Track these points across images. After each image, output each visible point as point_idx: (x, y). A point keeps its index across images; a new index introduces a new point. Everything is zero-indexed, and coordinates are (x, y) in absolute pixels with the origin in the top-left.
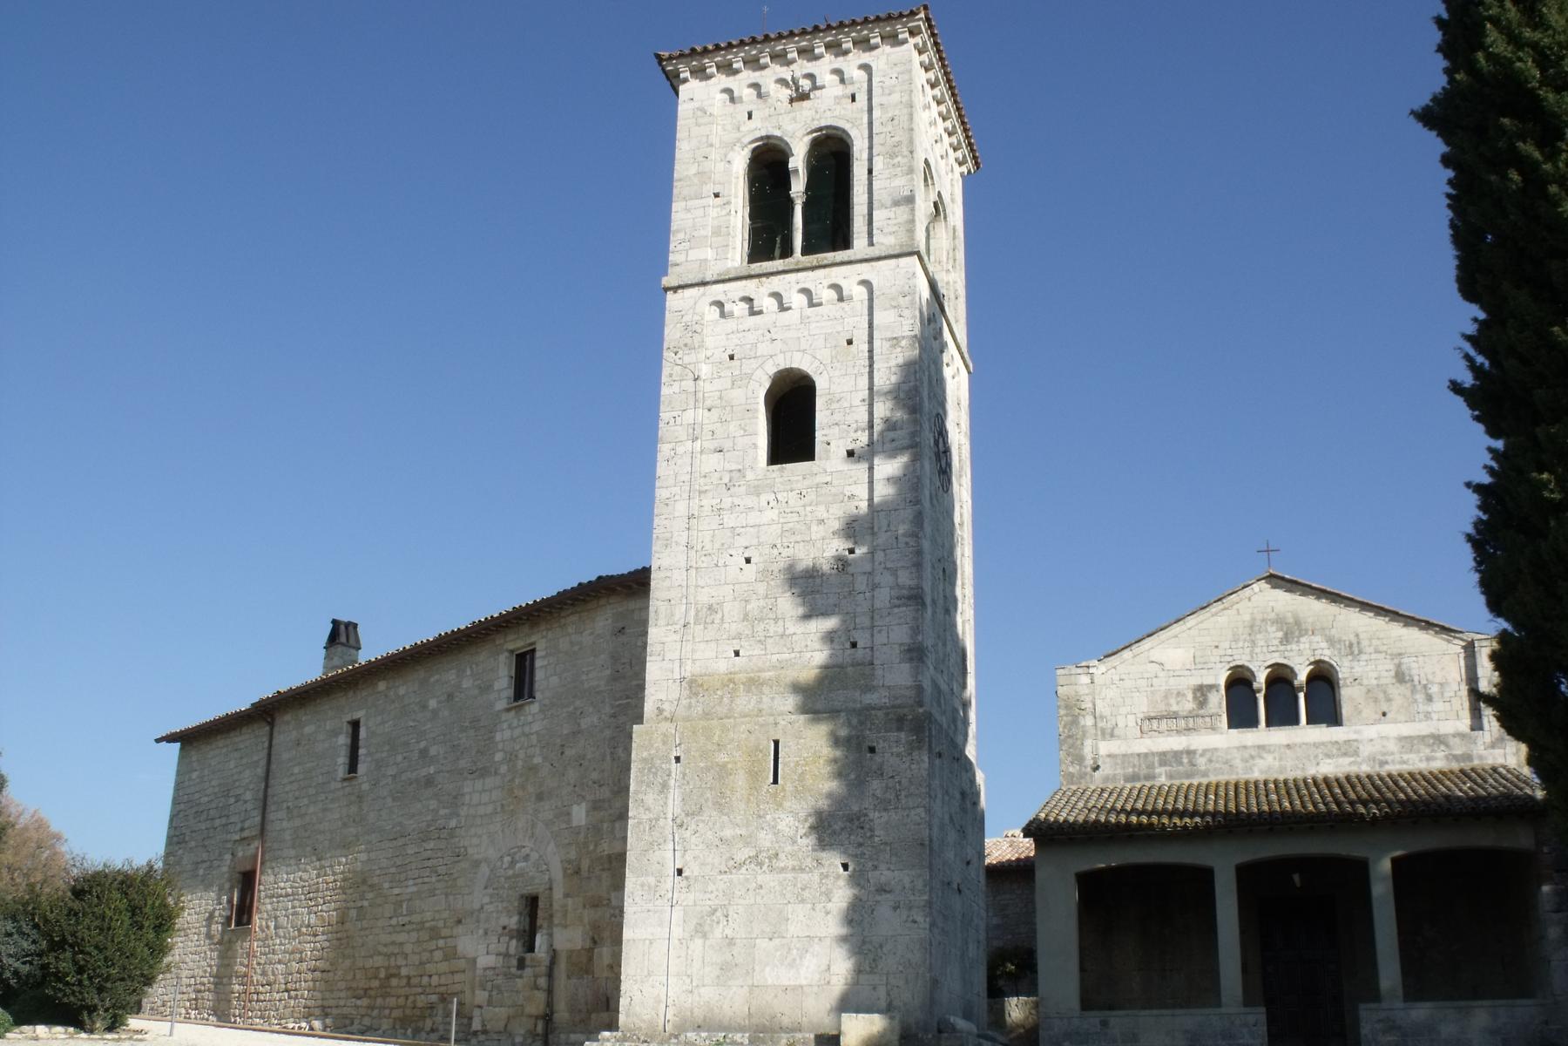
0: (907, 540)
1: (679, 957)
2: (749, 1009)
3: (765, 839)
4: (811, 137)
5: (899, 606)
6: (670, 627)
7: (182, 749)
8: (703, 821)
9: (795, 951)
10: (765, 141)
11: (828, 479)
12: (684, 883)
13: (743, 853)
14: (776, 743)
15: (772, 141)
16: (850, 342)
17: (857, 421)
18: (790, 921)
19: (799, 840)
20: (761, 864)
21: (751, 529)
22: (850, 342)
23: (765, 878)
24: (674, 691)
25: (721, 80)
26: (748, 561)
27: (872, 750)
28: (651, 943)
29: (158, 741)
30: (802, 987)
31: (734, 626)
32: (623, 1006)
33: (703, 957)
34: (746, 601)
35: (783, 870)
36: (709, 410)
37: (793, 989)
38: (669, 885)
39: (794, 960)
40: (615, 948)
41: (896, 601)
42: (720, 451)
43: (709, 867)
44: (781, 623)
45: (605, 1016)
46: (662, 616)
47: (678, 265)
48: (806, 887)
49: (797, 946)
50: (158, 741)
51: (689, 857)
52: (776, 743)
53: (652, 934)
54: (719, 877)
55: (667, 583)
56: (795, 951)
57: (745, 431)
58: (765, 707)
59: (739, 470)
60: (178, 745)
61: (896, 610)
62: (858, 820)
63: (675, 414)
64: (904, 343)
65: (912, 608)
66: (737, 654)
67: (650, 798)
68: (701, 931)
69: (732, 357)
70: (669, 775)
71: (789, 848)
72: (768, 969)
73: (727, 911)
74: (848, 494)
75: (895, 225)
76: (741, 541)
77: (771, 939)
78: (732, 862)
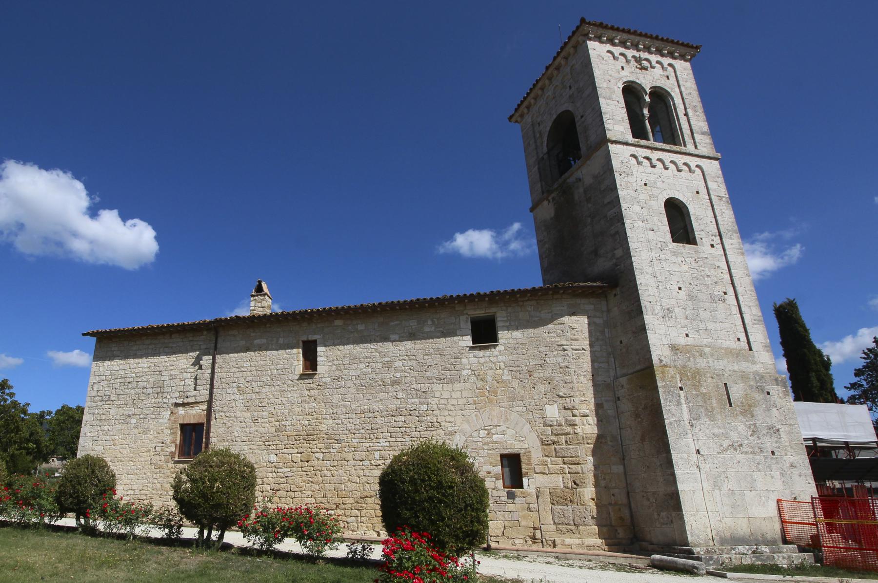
0: (751, 293)
1: (710, 501)
2: (751, 530)
3: (734, 436)
4: (623, 85)
5: (756, 324)
6: (654, 316)
7: (97, 342)
8: (703, 424)
9: (763, 498)
10: (628, 84)
11: (706, 256)
12: (702, 458)
13: (726, 443)
14: (725, 384)
15: (634, 85)
16: (698, 192)
17: (711, 231)
18: (757, 481)
19: (750, 438)
20: (735, 449)
21: (678, 273)
22: (698, 192)
23: (740, 457)
24: (667, 352)
25: (609, 47)
26: (680, 288)
27: (768, 393)
28: (694, 493)
29: (84, 335)
30: (771, 517)
31: (682, 321)
32: (688, 530)
33: (722, 501)
34: (685, 309)
35: (747, 453)
36: (642, 208)
37: (768, 519)
38: (695, 459)
39: (764, 503)
40: (71, 529)
41: (754, 321)
42: (652, 230)
43: (712, 449)
44: (703, 323)
45: (834, 525)
46: (649, 309)
47: (610, 130)
48: (759, 463)
49: (764, 495)
50: (84, 335)
51: (700, 443)
52: (725, 384)
53: (693, 487)
54: (719, 456)
55: (647, 293)
56: (763, 498)
57: (662, 223)
58: (711, 365)
59: (664, 242)
60: (95, 339)
61: (755, 326)
62: (773, 429)
63: (628, 206)
64: (724, 199)
65: (761, 326)
66: (687, 335)
67: (673, 409)
68: (716, 485)
69: (646, 185)
70: (679, 397)
71: (746, 441)
72: (754, 507)
73: (727, 475)
74: (717, 265)
75: (705, 143)
76: (674, 278)
77: (751, 491)
78: (722, 448)
